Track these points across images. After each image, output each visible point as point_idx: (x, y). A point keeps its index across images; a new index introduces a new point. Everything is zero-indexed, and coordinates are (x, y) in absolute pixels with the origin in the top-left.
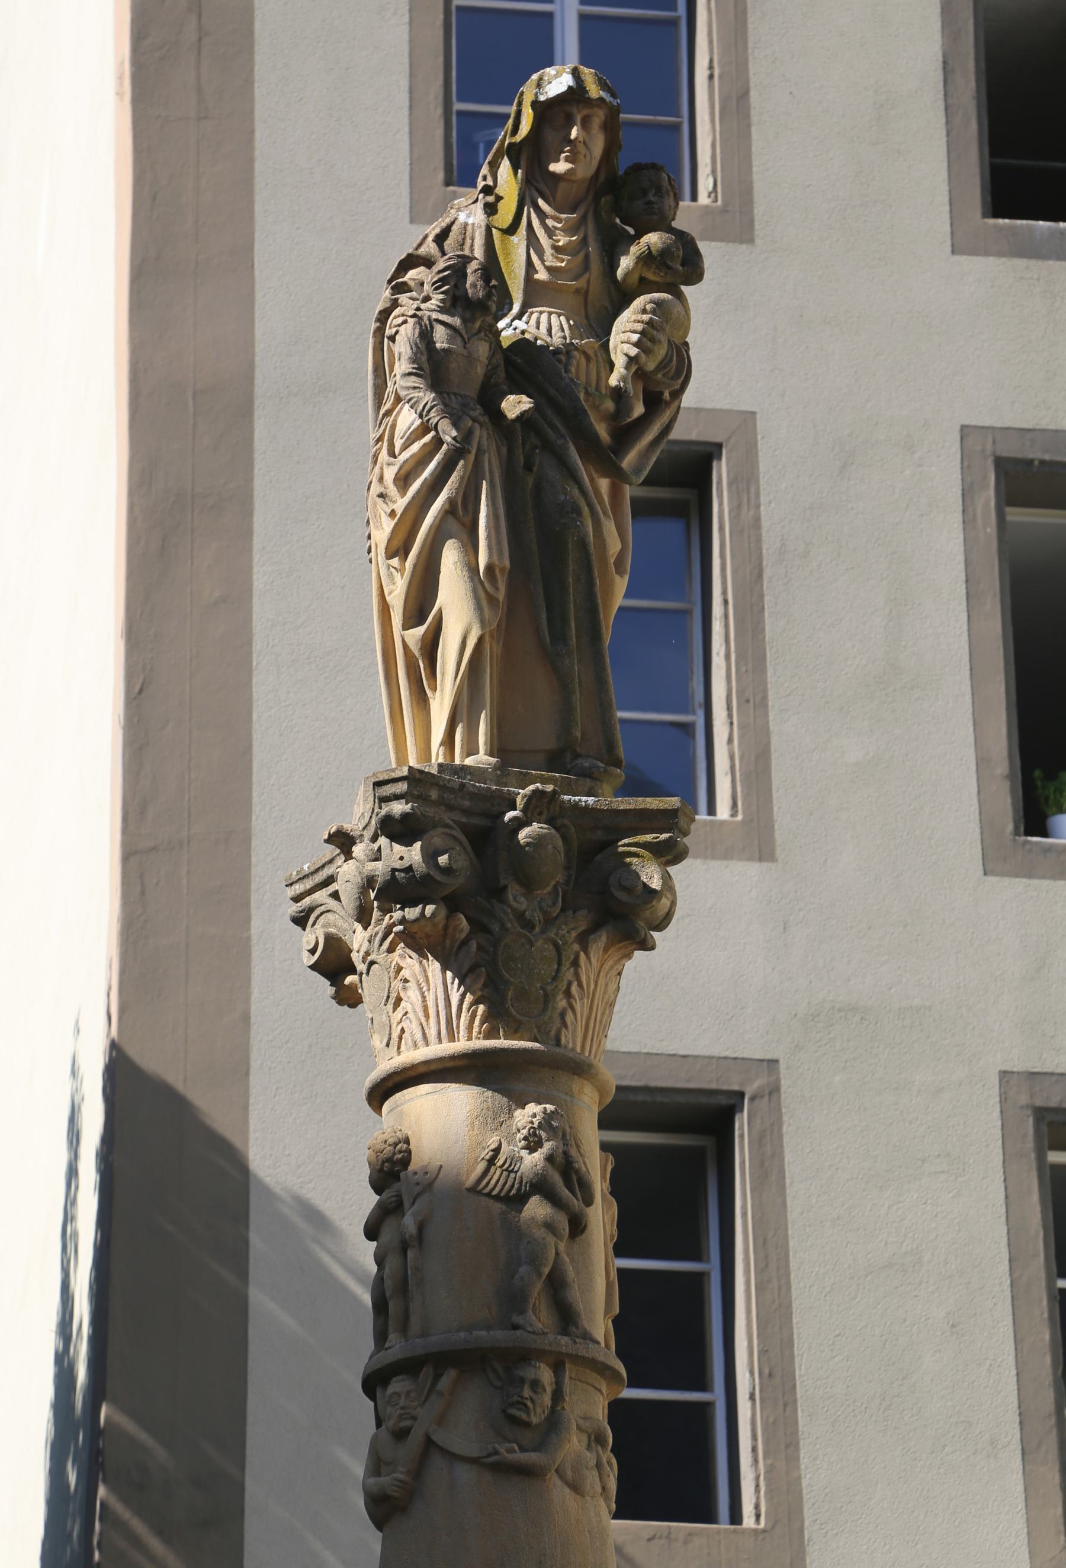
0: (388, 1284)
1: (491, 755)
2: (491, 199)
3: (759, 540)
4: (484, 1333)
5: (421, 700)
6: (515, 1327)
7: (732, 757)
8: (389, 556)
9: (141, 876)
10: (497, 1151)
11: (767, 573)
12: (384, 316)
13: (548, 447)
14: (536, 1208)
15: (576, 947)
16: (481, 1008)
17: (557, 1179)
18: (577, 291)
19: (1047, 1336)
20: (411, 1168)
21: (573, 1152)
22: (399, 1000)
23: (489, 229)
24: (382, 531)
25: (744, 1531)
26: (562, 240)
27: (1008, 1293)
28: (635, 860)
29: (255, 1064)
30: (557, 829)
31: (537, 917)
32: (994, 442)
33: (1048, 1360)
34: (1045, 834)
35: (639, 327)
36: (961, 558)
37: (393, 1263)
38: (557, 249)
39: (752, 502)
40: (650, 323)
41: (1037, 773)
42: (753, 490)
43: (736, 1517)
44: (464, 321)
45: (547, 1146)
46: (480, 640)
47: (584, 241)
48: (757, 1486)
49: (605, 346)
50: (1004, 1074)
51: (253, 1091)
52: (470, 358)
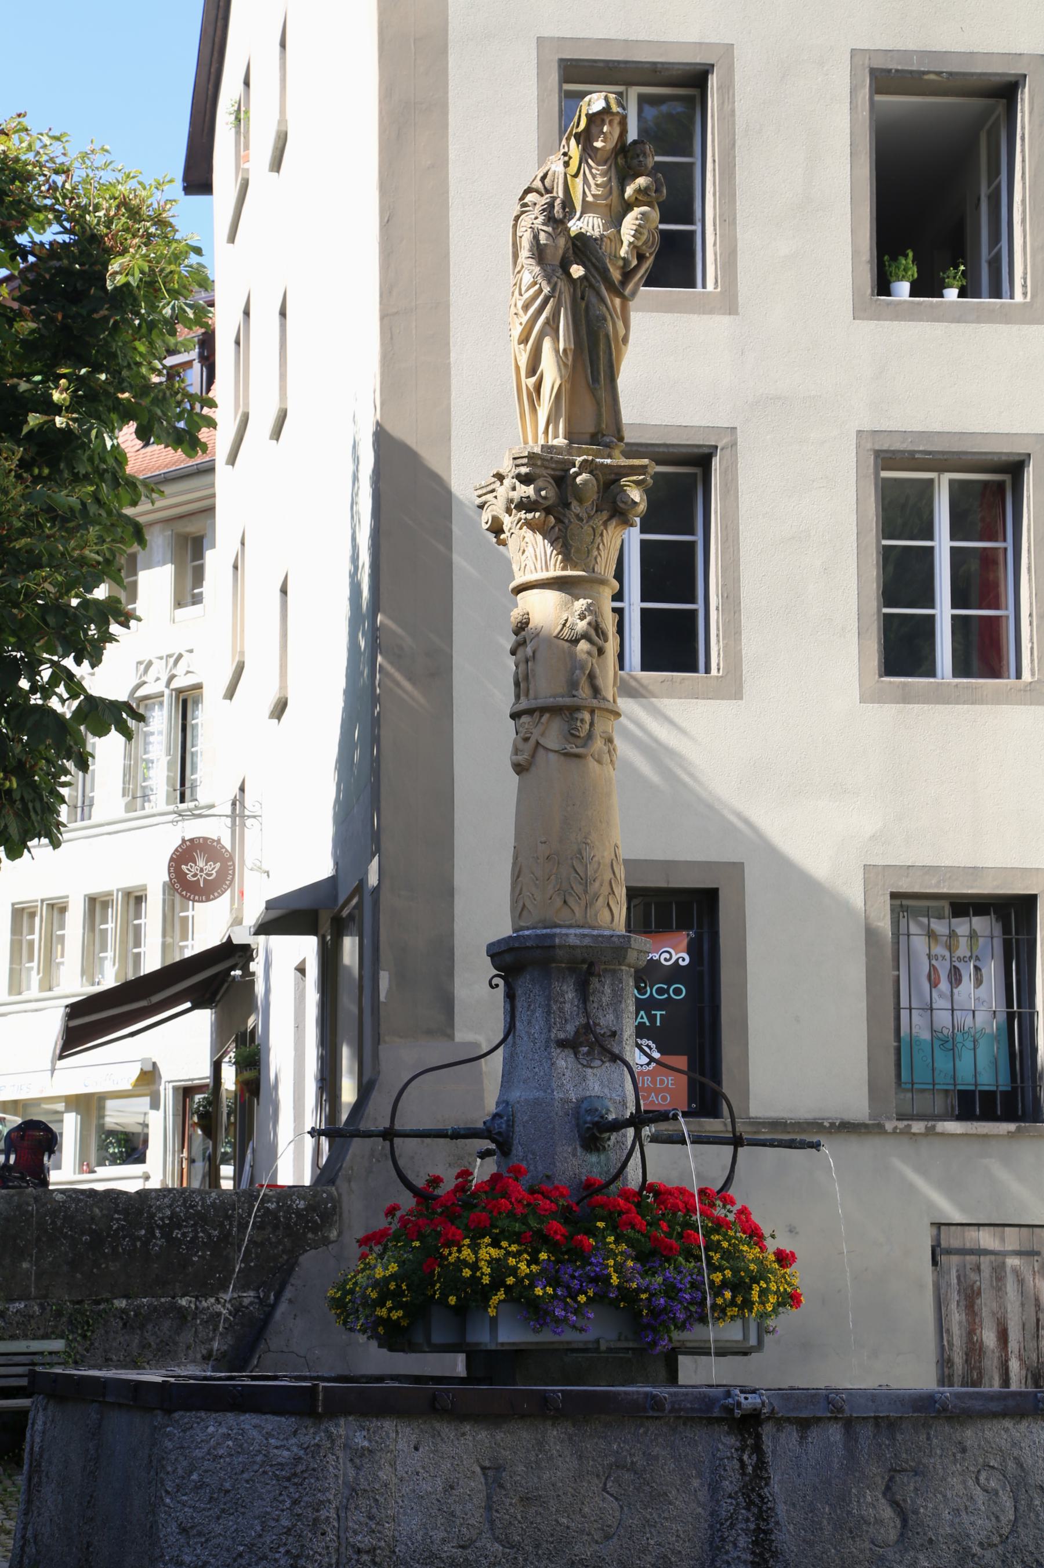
0: (520, 676)
1: (565, 439)
2: (566, 158)
3: (734, 124)
4: (561, 699)
5: (534, 409)
6: (574, 696)
7: (715, 254)
8: (519, 344)
9: (391, 329)
10: (567, 620)
11: (738, 143)
12: (517, 218)
13: (591, 286)
14: (583, 645)
15: (602, 527)
16: (560, 557)
17: (593, 633)
18: (606, 205)
19: (875, 573)
20: (530, 626)
21: (599, 620)
22: (524, 551)
23: (565, 174)
24: (517, 331)
25: (711, 677)
26: (600, 180)
27: (856, 551)
28: (628, 488)
29: (453, 434)
30: (594, 476)
31: (585, 516)
32: (870, 59)
33: (875, 585)
34: (889, 295)
35: (634, 227)
36: (848, 131)
37: (522, 667)
38: (597, 185)
39: (731, 100)
40: (639, 225)
41: (886, 258)
42: (731, 93)
43: (708, 670)
44: (554, 229)
45: (588, 618)
46: (560, 385)
47: (610, 180)
48: (719, 654)
49: (619, 232)
50: (859, 432)
51: (453, 448)
52: (556, 247)
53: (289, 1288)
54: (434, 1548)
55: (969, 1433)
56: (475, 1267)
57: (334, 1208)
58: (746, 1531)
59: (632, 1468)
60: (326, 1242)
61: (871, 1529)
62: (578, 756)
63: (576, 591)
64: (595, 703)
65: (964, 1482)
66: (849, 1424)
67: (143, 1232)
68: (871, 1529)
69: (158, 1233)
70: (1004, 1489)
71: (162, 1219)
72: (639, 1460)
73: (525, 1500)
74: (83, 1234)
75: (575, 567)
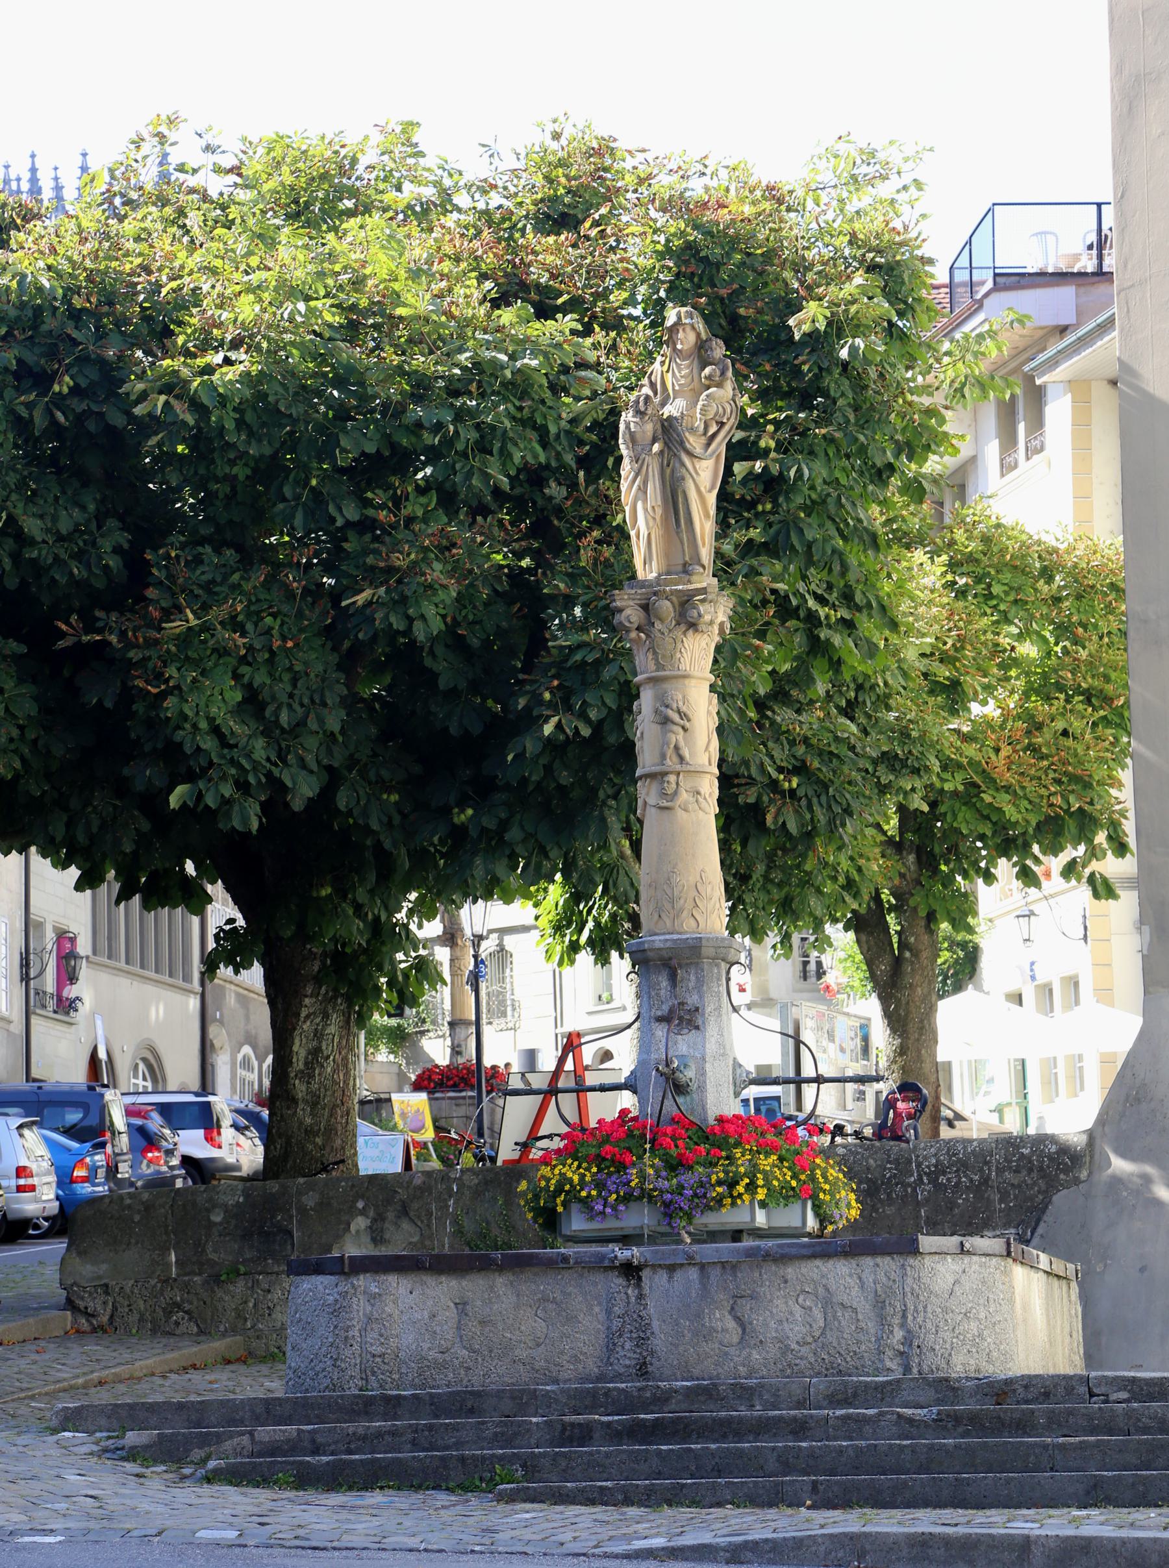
53: (1042, 1224)
55: (790, 1270)
56: (548, 1180)
58: (631, 1339)
59: (554, 1301)
60: (1077, 1181)
64: (678, 767)
66: (702, 1267)
69: (925, 1180)
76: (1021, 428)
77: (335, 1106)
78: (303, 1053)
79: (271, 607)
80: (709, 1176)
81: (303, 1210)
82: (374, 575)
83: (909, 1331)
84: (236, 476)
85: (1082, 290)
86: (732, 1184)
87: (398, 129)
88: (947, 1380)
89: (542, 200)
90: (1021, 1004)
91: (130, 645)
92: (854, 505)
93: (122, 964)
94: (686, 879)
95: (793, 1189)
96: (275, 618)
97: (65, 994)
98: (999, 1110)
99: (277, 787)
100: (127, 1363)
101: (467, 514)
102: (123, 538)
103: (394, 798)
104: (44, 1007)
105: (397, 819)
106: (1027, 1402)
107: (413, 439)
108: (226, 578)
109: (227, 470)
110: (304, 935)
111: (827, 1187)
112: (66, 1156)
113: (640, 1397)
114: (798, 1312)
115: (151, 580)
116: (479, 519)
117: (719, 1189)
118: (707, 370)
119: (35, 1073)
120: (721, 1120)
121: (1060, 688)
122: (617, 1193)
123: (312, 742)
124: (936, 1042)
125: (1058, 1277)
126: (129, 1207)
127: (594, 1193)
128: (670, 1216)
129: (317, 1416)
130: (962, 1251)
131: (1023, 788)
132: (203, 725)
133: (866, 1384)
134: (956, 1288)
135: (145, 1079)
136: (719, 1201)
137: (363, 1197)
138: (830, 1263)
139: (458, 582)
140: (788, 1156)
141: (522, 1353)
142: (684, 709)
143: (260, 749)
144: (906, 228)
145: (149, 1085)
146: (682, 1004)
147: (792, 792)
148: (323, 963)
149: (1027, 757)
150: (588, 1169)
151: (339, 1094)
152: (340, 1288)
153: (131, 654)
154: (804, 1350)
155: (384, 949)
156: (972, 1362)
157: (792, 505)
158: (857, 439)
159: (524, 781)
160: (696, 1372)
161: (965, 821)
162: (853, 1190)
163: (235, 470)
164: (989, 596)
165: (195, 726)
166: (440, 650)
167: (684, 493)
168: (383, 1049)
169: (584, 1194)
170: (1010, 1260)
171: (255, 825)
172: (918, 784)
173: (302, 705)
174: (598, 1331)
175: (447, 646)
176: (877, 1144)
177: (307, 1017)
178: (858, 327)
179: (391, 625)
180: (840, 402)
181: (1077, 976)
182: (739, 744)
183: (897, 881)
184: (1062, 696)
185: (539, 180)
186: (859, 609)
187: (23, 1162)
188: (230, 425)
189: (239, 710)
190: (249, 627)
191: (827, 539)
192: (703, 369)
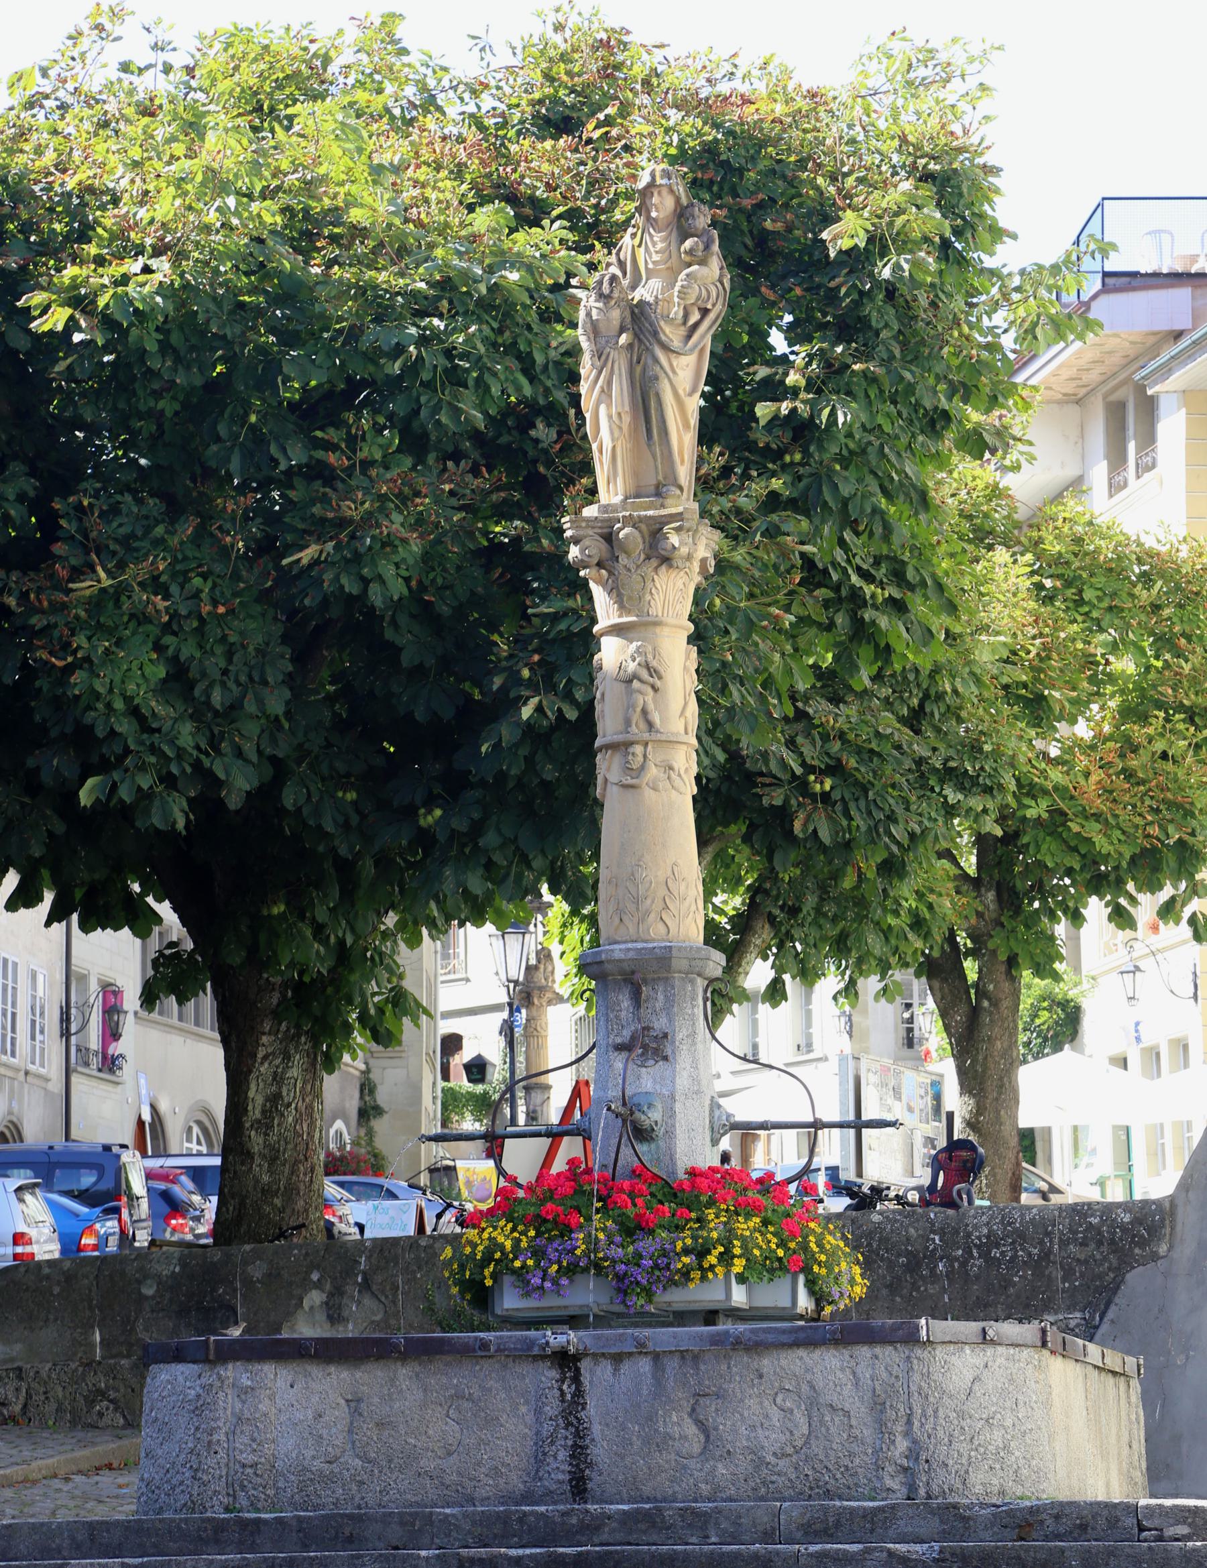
26: (660, 246)
53: (1113, 1308)
54: (306, 1463)
55: (766, 1362)
56: (474, 1246)
57: (1162, 1220)
59: (470, 1398)
60: (1155, 1257)
61: (677, 1444)
62: (632, 787)
63: (631, 635)
64: (646, 736)
65: (761, 1403)
66: (656, 1357)
67: (960, 1252)
68: (677, 1444)
70: (799, 1407)
71: (979, 1238)
72: (476, 1393)
73: (380, 1425)
74: (899, 1255)
75: (629, 613)
76: (1132, 447)
77: (297, 1162)
78: (260, 1100)
79: (200, 566)
80: (673, 1243)
81: (248, 1282)
82: (320, 529)
83: (915, 1442)
84: (162, 412)
85: (1199, 292)
86: (703, 1253)
87: (377, 22)
88: (955, 1506)
89: (541, 102)
90: (1125, 1068)
91: (34, 610)
92: (899, 454)
93: (175, 1021)
94: (655, 874)
95: (780, 1259)
96: (205, 579)
97: (110, 1051)
98: (1101, 1183)
99: (211, 781)
100: (24, 1462)
101: (437, 460)
102: (29, 485)
103: (351, 796)
104: (87, 1064)
105: (355, 820)
106: (1058, 1537)
107: (372, 368)
108: (148, 530)
109: (152, 404)
110: (258, 960)
111: (823, 1258)
112: (74, 1221)
113: (564, 1523)
114: (775, 1414)
115: (60, 533)
116: (450, 464)
117: (686, 1260)
118: (688, 244)
119: (74, 1134)
120: (693, 1173)
121: (1160, 705)
122: (559, 1263)
123: (252, 729)
124: (1017, 1102)
125: (1114, 1373)
126: (48, 1277)
127: (530, 1262)
128: (625, 1293)
129: (155, 1546)
130: (984, 1339)
131: (1116, 816)
132: (119, 705)
133: (852, 1510)
134: (976, 1387)
135: (199, 1143)
136: (686, 1274)
137: (318, 1267)
138: (817, 1354)
139: (421, 537)
140: (774, 1219)
141: (428, 1464)
142: (654, 663)
143: (186, 735)
144: (966, 132)
145: (204, 1149)
146: (647, 1028)
147: (825, 797)
148: (284, 996)
149: (1121, 783)
150: (524, 1233)
151: (302, 1147)
152: (203, 1380)
153: (33, 621)
154: (783, 1464)
155: (354, 978)
156: (995, 1481)
157: (827, 456)
158: (902, 378)
159: (502, 776)
160: (647, 1490)
161: (1050, 853)
162: (858, 1262)
163: (161, 404)
164: (1080, 602)
165: (109, 705)
166: (403, 619)
167: (658, 395)
168: (468, 1116)
169: (517, 1264)
170: (1046, 1353)
171: (181, 825)
172: (990, 805)
173: (238, 684)
174: (525, 1437)
175: (412, 616)
176: (920, 1210)
177: (265, 1058)
178: (904, 243)
179: (342, 587)
180: (884, 334)
181: (1186, 1038)
182: (752, 731)
183: (973, 921)
184: (1162, 714)
185: (538, 77)
186: (912, 588)
187: (22, 1228)
188: (151, 346)
189: (163, 688)
190: (174, 589)
191: (866, 496)
192: (682, 241)
